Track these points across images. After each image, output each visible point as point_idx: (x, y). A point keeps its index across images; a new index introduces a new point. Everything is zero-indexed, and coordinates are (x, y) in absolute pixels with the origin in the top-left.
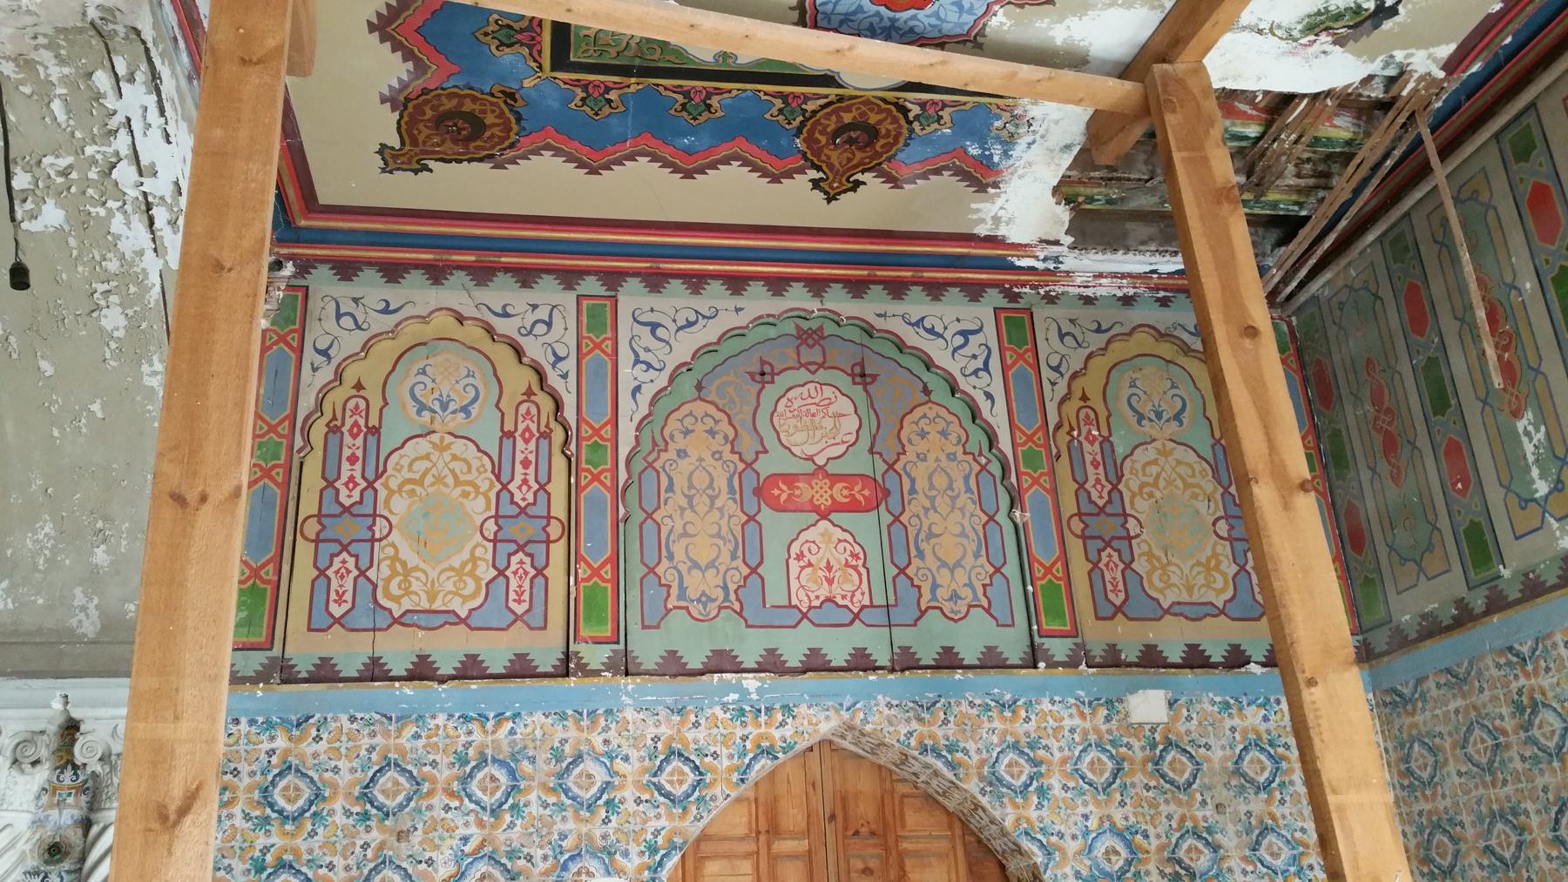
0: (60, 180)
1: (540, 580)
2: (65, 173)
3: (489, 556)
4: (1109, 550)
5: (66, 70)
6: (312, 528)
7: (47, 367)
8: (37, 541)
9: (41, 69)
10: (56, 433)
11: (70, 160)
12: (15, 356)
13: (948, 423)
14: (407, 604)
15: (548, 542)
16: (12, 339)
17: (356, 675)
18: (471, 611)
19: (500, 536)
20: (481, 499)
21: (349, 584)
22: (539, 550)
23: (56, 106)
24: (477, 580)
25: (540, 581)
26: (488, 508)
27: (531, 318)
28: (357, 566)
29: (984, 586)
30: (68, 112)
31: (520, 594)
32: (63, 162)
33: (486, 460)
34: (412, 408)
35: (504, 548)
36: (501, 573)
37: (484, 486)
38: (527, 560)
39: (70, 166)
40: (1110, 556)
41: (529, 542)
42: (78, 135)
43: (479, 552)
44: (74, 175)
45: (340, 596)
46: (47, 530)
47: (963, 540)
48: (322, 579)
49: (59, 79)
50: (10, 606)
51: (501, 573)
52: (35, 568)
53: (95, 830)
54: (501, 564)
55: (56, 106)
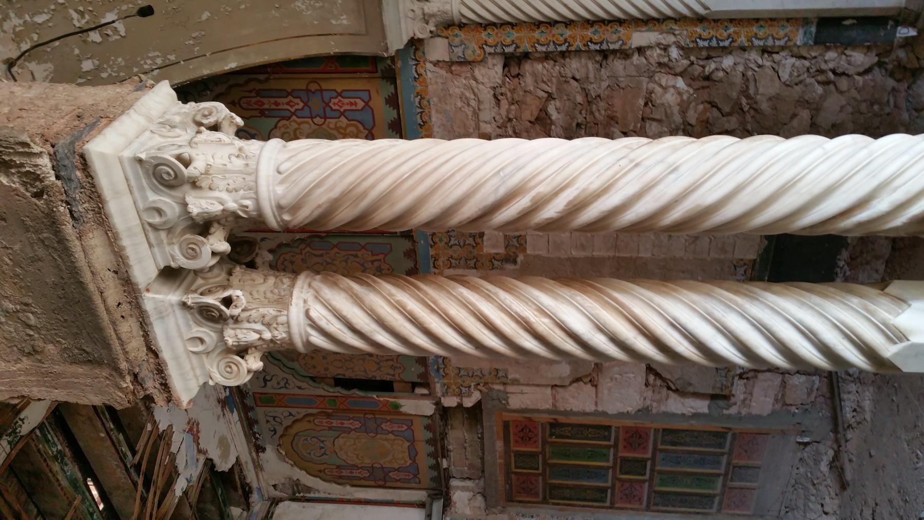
0: (87, 17)
1: (344, 94)
2: (82, 14)
3: (334, 121)
4: (331, 104)
5: (12, 15)
6: (313, 87)
7: (205, 15)
8: (307, 9)
9: (18, 29)
10: (243, 7)
11: (72, 12)
12: (203, 33)
13: (285, 260)
14: (408, 459)
15: (321, 90)
16: (194, 35)
17: (393, 86)
18: (365, 128)
19: (323, 115)
20: (302, 126)
21: (346, 101)
22: (327, 95)
23: (39, 19)
24: (348, 126)
25: (344, 94)
26: (307, 123)
27: (273, 422)
28: (336, 98)
29: (373, 255)
30: (41, 13)
31: (351, 104)
32: (75, 16)
33: (280, 124)
34: (324, 457)
35: (329, 113)
36: (342, 114)
37: (295, 125)
38: (333, 101)
39: (76, 11)
40: (334, 104)
41: (323, 101)
42: (53, 7)
43: (332, 126)
44: (81, 8)
45: (351, 104)
46: (300, 4)
47: (349, 261)
48: (346, 114)
49: (20, 18)
50: (345, 17)
51: (342, 114)
52: (322, 7)
53: (464, 21)
54: (337, 114)
55: (39, 19)
